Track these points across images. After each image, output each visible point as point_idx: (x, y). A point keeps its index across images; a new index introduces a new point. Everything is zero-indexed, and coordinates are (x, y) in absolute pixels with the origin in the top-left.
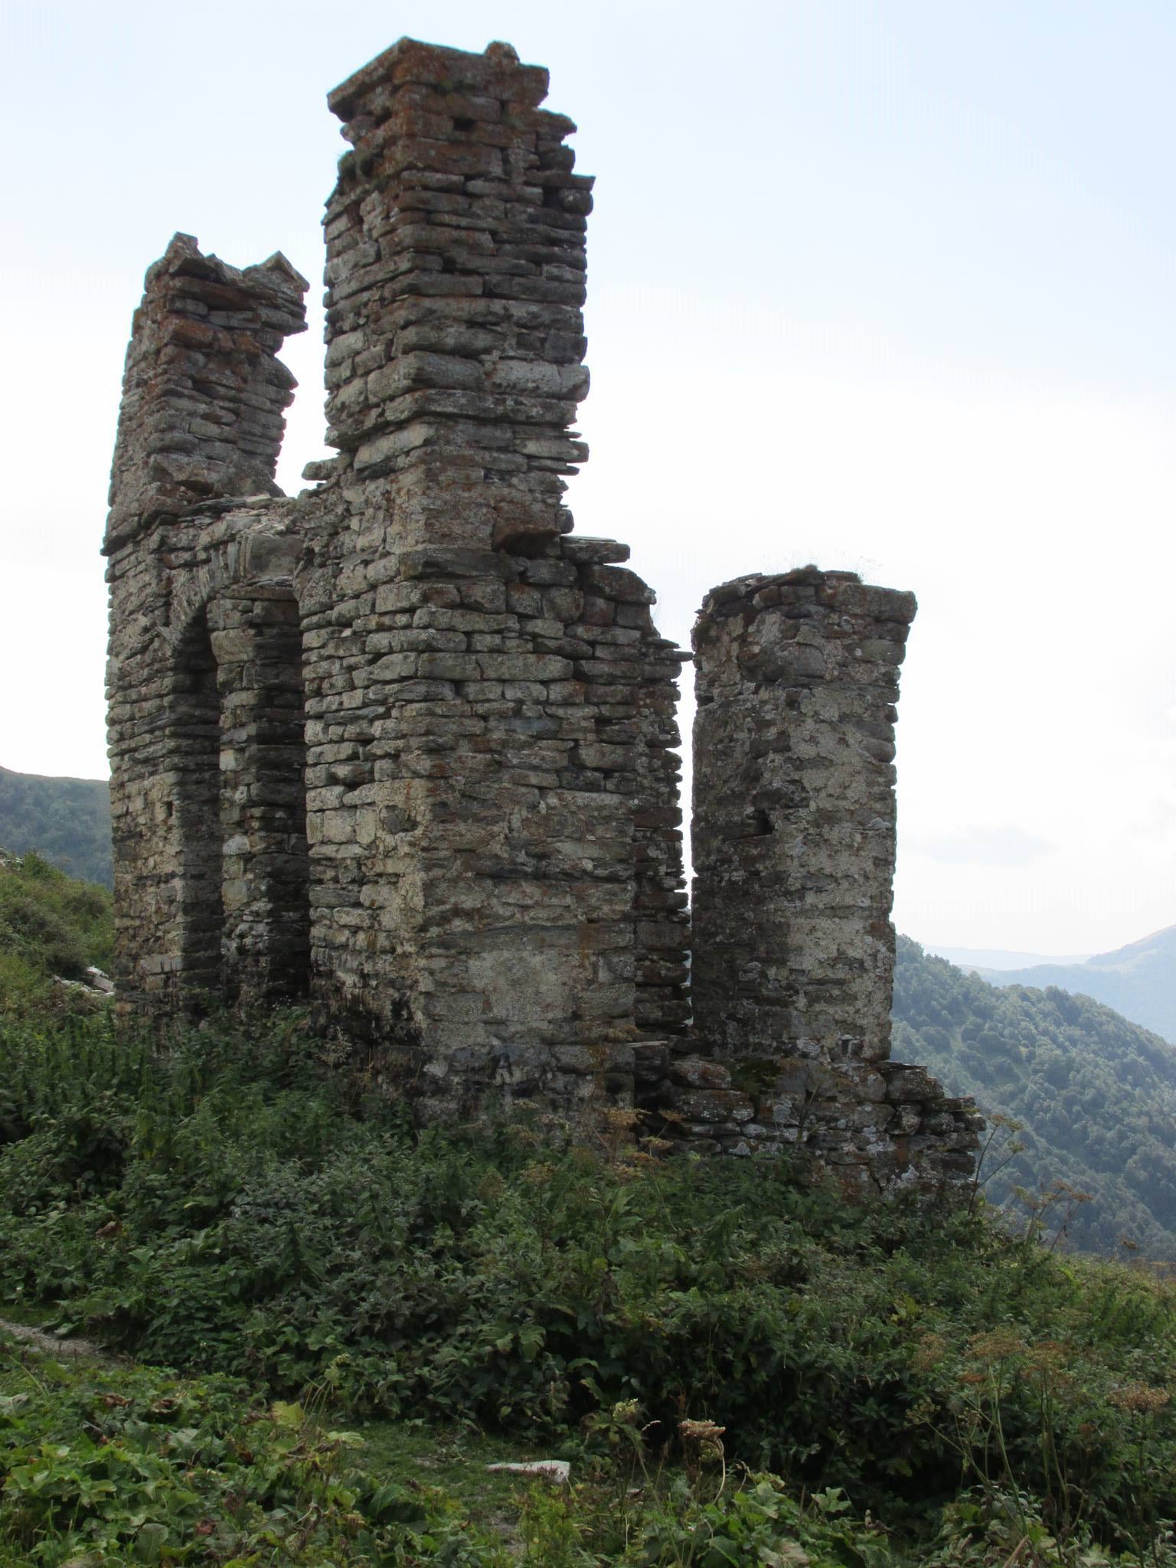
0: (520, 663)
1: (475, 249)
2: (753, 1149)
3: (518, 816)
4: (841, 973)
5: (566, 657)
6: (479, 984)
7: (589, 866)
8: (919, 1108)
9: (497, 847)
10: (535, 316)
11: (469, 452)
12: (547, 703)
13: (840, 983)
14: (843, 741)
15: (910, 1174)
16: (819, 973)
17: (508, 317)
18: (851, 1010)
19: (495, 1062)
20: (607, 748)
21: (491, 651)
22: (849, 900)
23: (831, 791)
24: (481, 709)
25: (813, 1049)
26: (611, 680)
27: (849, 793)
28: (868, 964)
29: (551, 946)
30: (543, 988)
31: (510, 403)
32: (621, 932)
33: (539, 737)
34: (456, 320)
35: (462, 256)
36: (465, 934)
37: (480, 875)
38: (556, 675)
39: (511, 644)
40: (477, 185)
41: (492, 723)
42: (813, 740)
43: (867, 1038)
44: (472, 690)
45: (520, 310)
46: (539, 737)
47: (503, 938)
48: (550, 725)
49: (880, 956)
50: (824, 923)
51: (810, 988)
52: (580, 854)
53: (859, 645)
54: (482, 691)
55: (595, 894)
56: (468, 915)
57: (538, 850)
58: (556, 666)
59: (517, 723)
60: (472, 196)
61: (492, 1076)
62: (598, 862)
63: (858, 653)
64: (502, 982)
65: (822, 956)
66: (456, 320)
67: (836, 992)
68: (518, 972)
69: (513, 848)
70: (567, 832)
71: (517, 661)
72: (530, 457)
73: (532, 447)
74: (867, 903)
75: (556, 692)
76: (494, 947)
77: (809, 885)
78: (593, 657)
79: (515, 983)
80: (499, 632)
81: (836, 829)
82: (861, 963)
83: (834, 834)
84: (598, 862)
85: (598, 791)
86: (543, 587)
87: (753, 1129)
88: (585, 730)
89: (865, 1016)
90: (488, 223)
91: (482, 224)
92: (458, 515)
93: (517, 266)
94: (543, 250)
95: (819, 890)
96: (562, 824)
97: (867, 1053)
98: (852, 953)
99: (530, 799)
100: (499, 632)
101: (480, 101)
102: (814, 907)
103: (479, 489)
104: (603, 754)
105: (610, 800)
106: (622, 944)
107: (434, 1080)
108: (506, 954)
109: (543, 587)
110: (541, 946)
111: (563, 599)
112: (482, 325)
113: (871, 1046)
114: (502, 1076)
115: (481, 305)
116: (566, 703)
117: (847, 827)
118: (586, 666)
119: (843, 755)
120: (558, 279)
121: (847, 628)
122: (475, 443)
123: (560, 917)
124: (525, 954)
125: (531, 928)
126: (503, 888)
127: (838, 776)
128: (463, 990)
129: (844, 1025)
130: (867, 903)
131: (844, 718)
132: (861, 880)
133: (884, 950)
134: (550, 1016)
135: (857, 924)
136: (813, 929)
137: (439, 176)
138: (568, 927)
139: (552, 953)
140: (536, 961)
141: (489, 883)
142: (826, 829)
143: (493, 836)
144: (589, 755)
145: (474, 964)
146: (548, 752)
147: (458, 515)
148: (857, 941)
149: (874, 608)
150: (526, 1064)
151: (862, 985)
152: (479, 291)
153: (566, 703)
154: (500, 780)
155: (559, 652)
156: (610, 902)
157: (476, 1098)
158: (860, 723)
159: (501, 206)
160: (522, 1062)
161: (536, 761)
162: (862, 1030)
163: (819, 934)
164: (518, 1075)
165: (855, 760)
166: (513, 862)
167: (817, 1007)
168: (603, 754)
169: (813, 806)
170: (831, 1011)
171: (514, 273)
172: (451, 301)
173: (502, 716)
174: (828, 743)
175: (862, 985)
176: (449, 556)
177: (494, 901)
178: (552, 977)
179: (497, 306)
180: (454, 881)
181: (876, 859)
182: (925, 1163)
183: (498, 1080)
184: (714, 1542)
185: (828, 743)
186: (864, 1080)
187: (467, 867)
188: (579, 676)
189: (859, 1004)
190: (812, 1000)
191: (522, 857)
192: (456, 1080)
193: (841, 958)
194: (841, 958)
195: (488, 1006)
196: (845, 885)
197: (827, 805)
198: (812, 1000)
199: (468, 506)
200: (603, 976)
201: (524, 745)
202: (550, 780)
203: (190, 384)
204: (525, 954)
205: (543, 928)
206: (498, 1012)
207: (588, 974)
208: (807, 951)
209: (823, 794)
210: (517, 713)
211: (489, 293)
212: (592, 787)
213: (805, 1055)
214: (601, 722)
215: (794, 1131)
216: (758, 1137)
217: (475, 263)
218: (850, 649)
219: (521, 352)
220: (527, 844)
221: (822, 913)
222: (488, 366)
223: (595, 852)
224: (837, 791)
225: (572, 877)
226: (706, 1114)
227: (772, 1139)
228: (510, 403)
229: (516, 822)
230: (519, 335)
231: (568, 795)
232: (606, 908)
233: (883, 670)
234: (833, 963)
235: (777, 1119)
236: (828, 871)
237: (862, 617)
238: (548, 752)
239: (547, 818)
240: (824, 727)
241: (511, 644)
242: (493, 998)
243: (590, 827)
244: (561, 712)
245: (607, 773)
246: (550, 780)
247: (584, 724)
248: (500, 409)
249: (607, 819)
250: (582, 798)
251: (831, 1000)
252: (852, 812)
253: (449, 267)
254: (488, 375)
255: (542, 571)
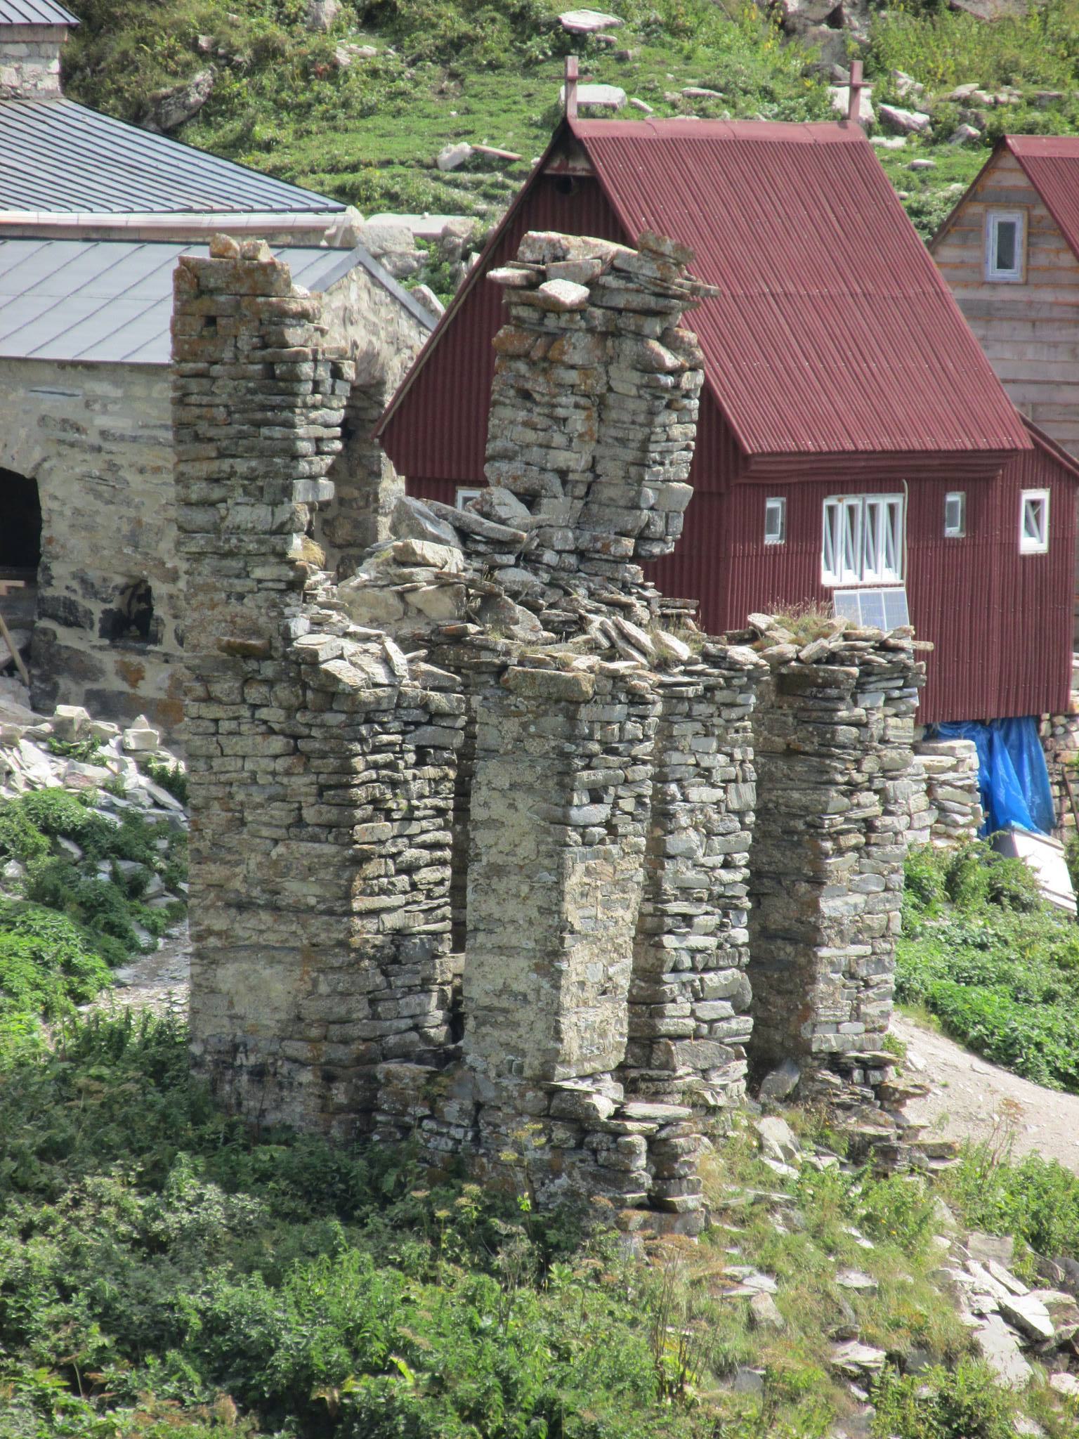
0: (250, 742)
1: (213, 422)
2: (427, 1141)
3: (254, 860)
4: (505, 1003)
5: (286, 736)
6: (224, 987)
7: (312, 901)
8: (575, 1126)
9: (237, 884)
10: (253, 470)
11: (212, 580)
12: (274, 774)
13: (505, 1011)
14: (512, 806)
15: (563, 1181)
16: (486, 1001)
17: (232, 474)
18: (515, 1035)
19: (235, 1048)
20: (325, 808)
21: (230, 733)
22: (514, 942)
23: (501, 848)
24: (223, 778)
25: (480, 1065)
26: (323, 755)
27: (519, 851)
28: (531, 997)
29: (280, 962)
30: (273, 994)
31: (234, 541)
32: (336, 956)
33: (272, 799)
34: (199, 478)
35: (203, 428)
36: (216, 949)
37: (228, 905)
38: (278, 751)
39: (244, 728)
40: (216, 370)
41: (234, 789)
42: (486, 805)
43: (527, 1060)
44: (216, 763)
45: (242, 466)
46: (272, 799)
47: (244, 954)
48: (280, 789)
49: (543, 992)
50: (490, 959)
51: (479, 1013)
52: (305, 891)
53: (534, 723)
54: (223, 764)
55: (316, 923)
56: (219, 934)
57: (270, 887)
58: (278, 744)
59: (254, 789)
60: (214, 379)
61: (234, 1058)
62: (321, 899)
63: (532, 729)
64: (242, 987)
65: (489, 987)
66: (199, 478)
67: (501, 1019)
68: (253, 981)
69: (251, 885)
70: (293, 873)
71: (250, 741)
72: (260, 581)
73: (258, 573)
74: (531, 945)
75: (280, 765)
76: (235, 960)
77: (482, 926)
78: (309, 737)
79: (251, 989)
80: (236, 718)
81: (505, 880)
82: (525, 996)
83: (500, 885)
84: (321, 899)
85: (320, 841)
86: (270, 683)
87: (428, 1124)
88: (307, 794)
89: (526, 1041)
90: (224, 398)
91: (217, 401)
92: (204, 630)
93: (240, 432)
94: (259, 416)
95: (491, 932)
96: (288, 868)
97: (528, 1073)
98: (515, 987)
99: (263, 847)
100: (236, 718)
101: (222, 299)
102: (482, 947)
103: (220, 608)
104: (320, 813)
105: (328, 849)
106: (336, 965)
107: (194, 1057)
108: (245, 966)
109: (270, 683)
110: (272, 962)
111: (283, 692)
112: (217, 481)
113: (531, 1067)
114: (240, 1059)
115: (215, 465)
116: (288, 773)
117: (514, 879)
118: (301, 744)
119: (511, 817)
120: (270, 438)
121: (522, 708)
122: (217, 572)
123: (286, 940)
124: (258, 967)
125: (265, 947)
126: (245, 915)
127: (507, 835)
128: (213, 991)
129: (506, 1046)
130: (531, 945)
131: (513, 786)
132: (526, 926)
133: (547, 986)
134: (277, 1017)
135: (522, 963)
136: (481, 965)
137: (191, 365)
138: (293, 949)
139: (279, 968)
140: (267, 973)
141: (233, 911)
142: (495, 879)
143: (235, 875)
144: (309, 815)
145: (221, 973)
146: (279, 812)
147: (204, 630)
148: (522, 976)
149: (544, 690)
150: (258, 1051)
151: (525, 1015)
152: (214, 454)
153: (288, 773)
154: (240, 833)
155: (282, 733)
156: (328, 930)
157: (222, 1074)
158: (530, 789)
159: (232, 384)
160: (256, 1050)
161: (265, 819)
162: (523, 1054)
163: (487, 969)
164: (252, 1060)
165: (524, 822)
166: (249, 896)
167: (484, 1030)
168: (320, 813)
169: (484, 862)
170: (496, 1033)
171: (242, 436)
172: (197, 464)
173: (243, 784)
174: (498, 809)
175: (525, 1015)
176: (197, 661)
177: (236, 925)
178: (279, 986)
179: (226, 465)
180: (206, 909)
181: (540, 908)
182: (576, 1173)
183: (238, 1062)
184: (346, 1401)
185: (498, 809)
186: (522, 1096)
187: (219, 898)
188: (295, 751)
189: (522, 1031)
190: (481, 1023)
191: (256, 892)
192: (209, 1058)
193: (505, 990)
194: (505, 990)
195: (231, 1004)
196: (511, 929)
197: (500, 860)
198: (481, 1023)
199: (211, 622)
200: (323, 988)
201: (261, 806)
202: (281, 833)
203: (512, 393)
204: (258, 967)
205: (274, 948)
206: (239, 1010)
207: (309, 987)
208: (474, 982)
209: (494, 850)
210: (254, 781)
211: (222, 455)
212: (314, 839)
213: (473, 1069)
214: (322, 789)
215: (461, 1131)
216: (430, 1131)
217: (212, 433)
218: (525, 726)
219: (246, 499)
220: (262, 882)
221: (490, 951)
222: (223, 512)
223: (317, 890)
224: (507, 849)
225: (301, 911)
226: (385, 1107)
227: (441, 1134)
228: (234, 541)
229: (252, 866)
230: (243, 486)
231: (294, 845)
232: (323, 936)
233: (553, 744)
234: (499, 994)
235: (449, 1119)
236: (496, 916)
237: (534, 698)
238: (279, 812)
239: (275, 863)
240: (496, 794)
241: (244, 728)
242: (235, 999)
243: (311, 870)
244: (285, 780)
245: (329, 827)
246: (281, 833)
247: (303, 790)
248: (227, 547)
249: (327, 865)
250: (306, 847)
251: (495, 1025)
252: (521, 867)
253: (197, 438)
254: (223, 519)
255: (268, 669)
